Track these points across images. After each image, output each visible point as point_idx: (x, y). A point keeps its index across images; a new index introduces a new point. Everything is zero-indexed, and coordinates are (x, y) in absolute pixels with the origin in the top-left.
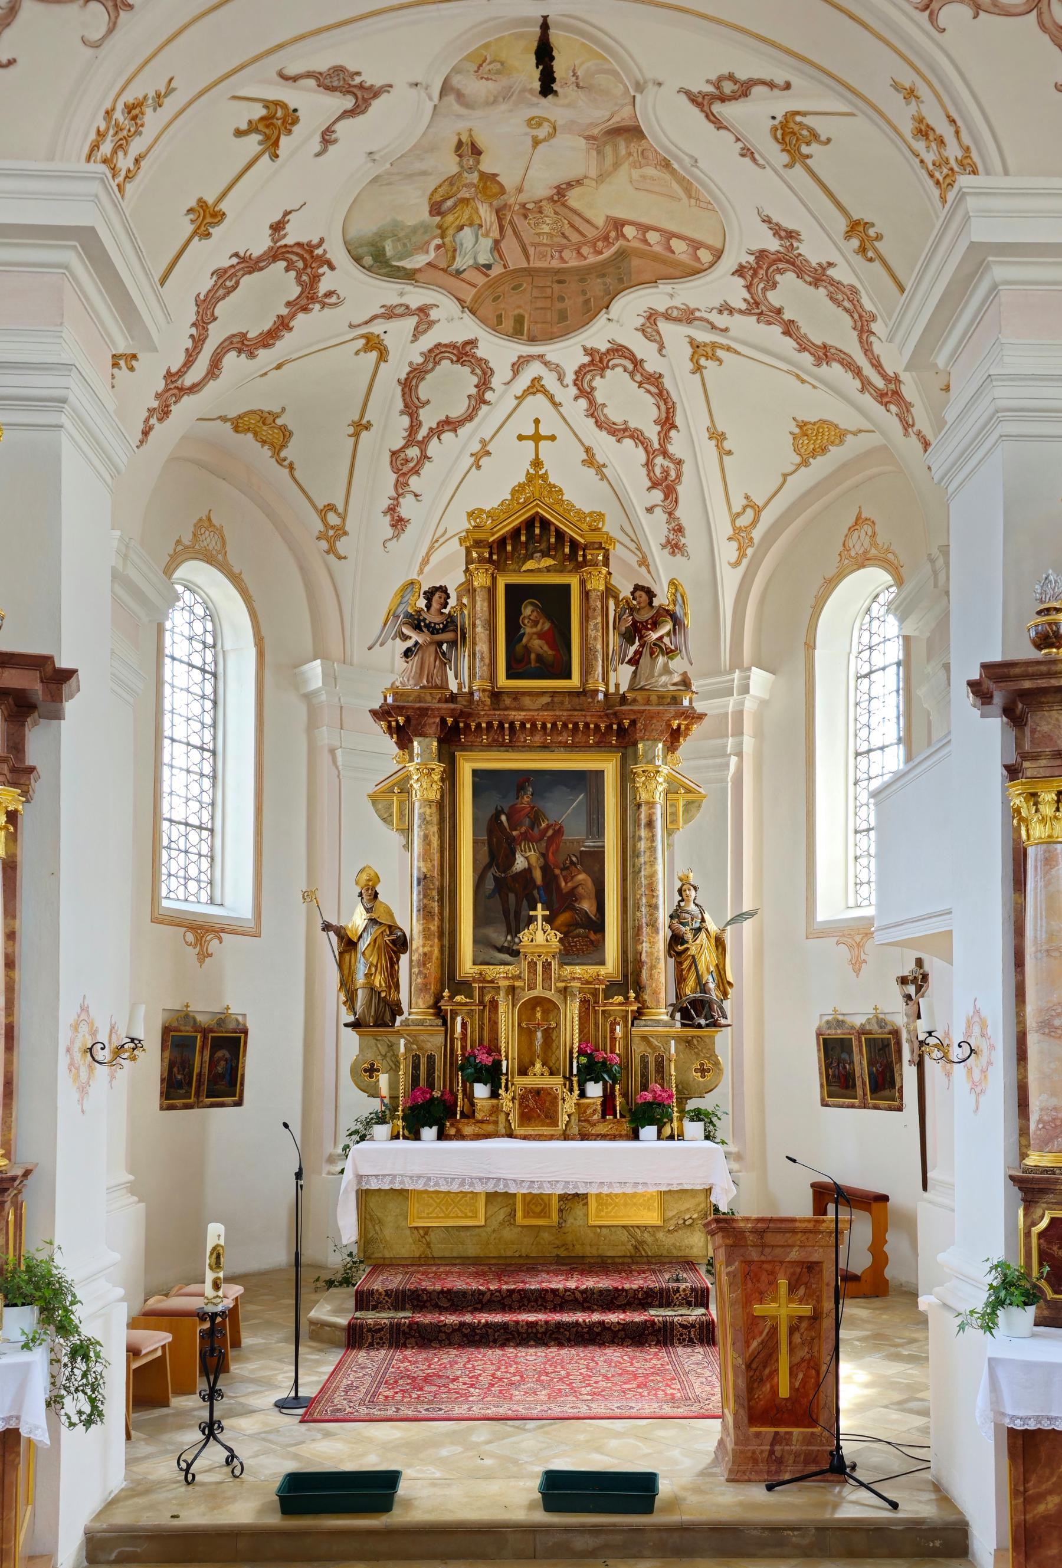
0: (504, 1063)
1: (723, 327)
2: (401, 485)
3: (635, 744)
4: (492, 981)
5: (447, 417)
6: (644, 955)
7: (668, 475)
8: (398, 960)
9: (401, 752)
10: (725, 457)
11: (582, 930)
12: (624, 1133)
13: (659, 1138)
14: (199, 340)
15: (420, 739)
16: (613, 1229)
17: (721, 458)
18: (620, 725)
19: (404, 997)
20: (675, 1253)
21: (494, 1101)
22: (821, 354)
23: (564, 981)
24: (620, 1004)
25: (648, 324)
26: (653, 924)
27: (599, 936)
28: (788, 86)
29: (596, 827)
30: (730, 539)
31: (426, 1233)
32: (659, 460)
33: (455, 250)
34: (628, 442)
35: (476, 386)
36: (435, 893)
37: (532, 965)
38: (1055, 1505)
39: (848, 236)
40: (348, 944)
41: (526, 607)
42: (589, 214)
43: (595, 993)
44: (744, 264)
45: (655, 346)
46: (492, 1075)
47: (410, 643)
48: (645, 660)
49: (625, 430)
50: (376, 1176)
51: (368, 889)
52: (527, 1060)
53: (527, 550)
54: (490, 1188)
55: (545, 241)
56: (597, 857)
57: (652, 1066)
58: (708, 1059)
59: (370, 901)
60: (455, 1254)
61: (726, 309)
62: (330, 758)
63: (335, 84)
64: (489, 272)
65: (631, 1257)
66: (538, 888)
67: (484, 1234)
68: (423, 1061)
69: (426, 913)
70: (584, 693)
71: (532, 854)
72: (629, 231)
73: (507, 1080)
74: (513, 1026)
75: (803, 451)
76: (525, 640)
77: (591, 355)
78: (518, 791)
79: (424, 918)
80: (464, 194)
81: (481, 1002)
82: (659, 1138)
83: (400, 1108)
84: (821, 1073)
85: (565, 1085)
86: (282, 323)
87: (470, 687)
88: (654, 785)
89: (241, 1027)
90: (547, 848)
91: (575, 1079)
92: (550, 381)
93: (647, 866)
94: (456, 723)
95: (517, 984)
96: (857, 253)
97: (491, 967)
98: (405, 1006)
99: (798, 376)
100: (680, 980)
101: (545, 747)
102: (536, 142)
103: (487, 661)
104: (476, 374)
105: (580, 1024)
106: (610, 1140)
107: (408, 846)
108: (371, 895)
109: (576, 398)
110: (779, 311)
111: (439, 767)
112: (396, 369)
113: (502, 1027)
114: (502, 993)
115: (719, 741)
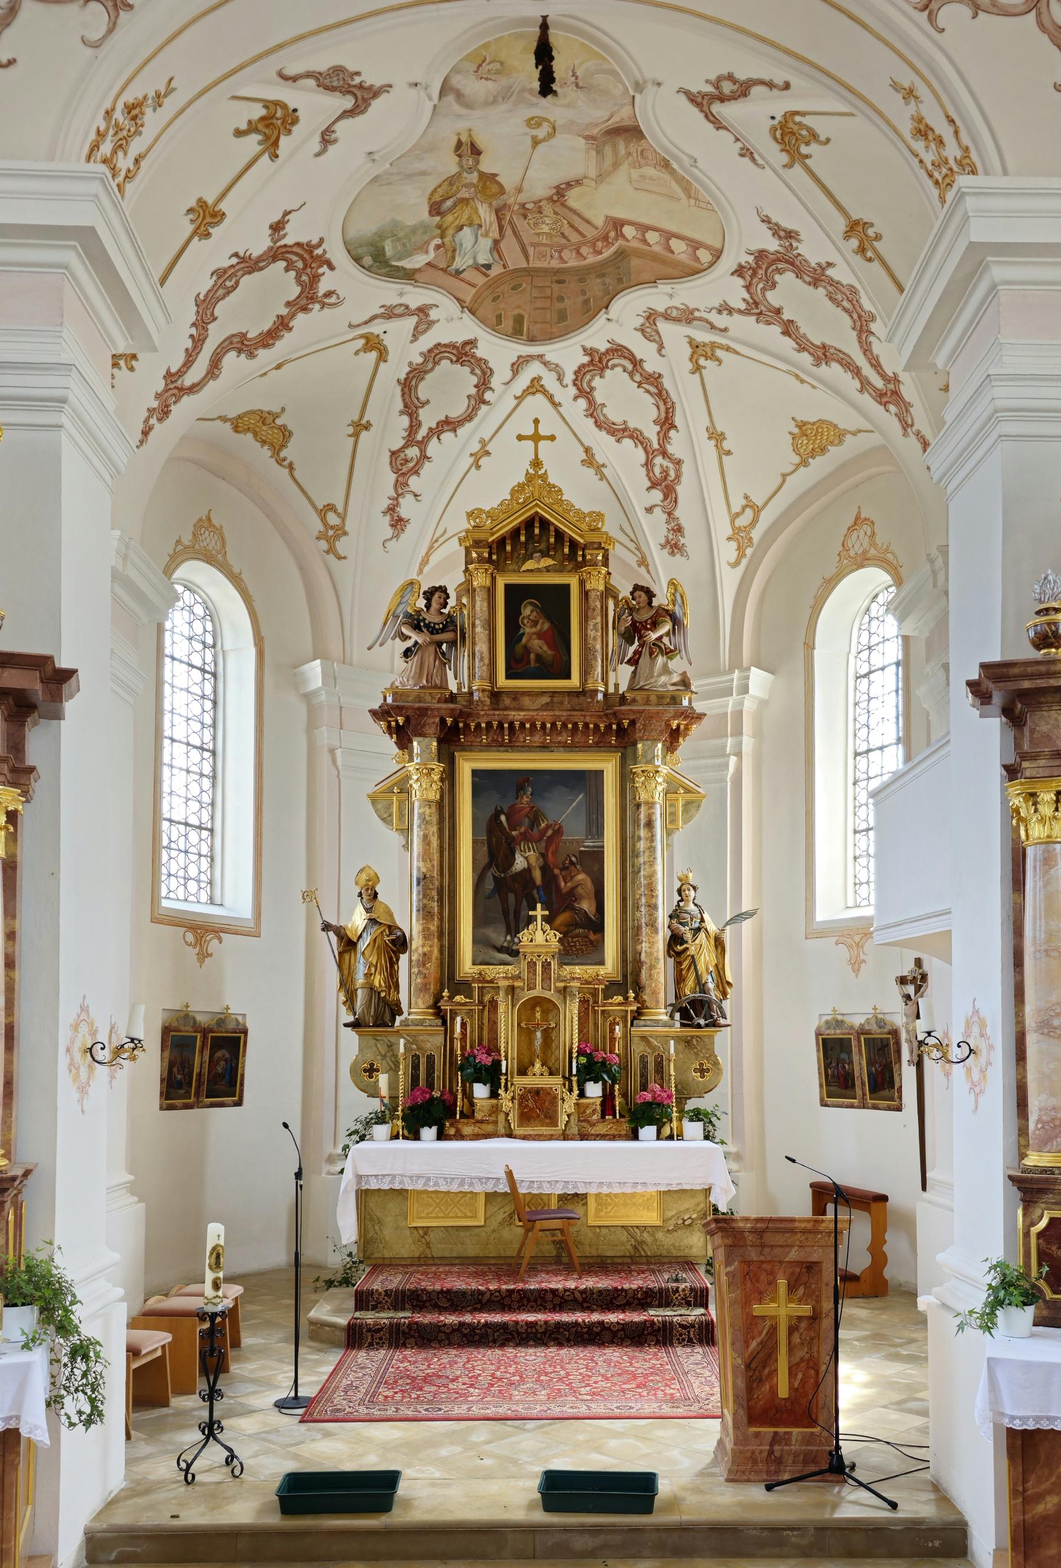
0: (504, 1063)
1: (723, 327)
2: (401, 485)
3: (635, 744)
4: (492, 981)
5: (447, 417)
6: (643, 955)
7: (668, 475)
8: (398, 960)
10: (724, 457)
11: (581, 930)
12: (623, 1133)
13: (658, 1138)
14: (199, 340)
15: (420, 739)
16: (612, 1229)
17: (720, 458)
18: (619, 725)
19: (403, 997)
20: (675, 1253)
21: (494, 1101)
22: (820, 354)
23: (563, 981)
24: (619, 1004)
25: (648, 324)
26: (652, 924)
27: (598, 936)
28: (787, 86)
29: (596, 827)
30: (729, 539)
31: (426, 1233)
32: (659, 460)
33: (454, 250)
34: (628, 443)
35: (476, 386)
36: (434, 893)
37: (532, 965)
38: (1054, 1505)
39: (847, 236)
40: (348, 944)
41: (525, 607)
42: (588, 214)
43: (594, 993)
44: (743, 264)
45: (654, 346)
46: (491, 1075)
47: (409, 643)
48: (644, 660)
49: (624, 430)
50: (376, 1176)
51: (367, 889)
53: (526, 550)
54: (490, 1188)
55: (544, 241)
56: (596, 857)
57: (651, 1066)
58: (707, 1059)
59: (369, 901)
60: (454, 1255)
61: (725, 309)
63: (335, 84)
64: (488, 272)
65: (630, 1257)
66: (538, 888)
68: (423, 1061)
69: (426, 913)
70: (584, 693)
71: (532, 854)
72: (629, 231)
73: (506, 1080)
74: (512, 1026)
75: (802, 451)
76: (524, 640)
77: (590, 355)
78: (518, 791)
79: (424, 918)
80: (464, 194)
82: (658, 1138)
83: (400, 1109)
84: (820, 1073)
85: (564, 1085)
86: (282, 323)
87: (470, 687)
88: (653, 785)
89: (240, 1027)
90: (547, 848)
91: (574, 1079)
92: (549, 381)
93: (647, 866)
94: (456, 722)
95: (516, 984)
96: (857, 253)
97: (491, 967)
98: (404, 1006)
99: (797, 376)
100: (680, 980)
101: (544, 747)
102: (536, 142)
103: (487, 661)
104: (475, 374)
105: (580, 1024)
106: (610, 1140)
107: (407, 846)
108: (370, 895)
109: (576, 398)
110: (778, 311)
111: (438, 767)
112: (395, 369)
114: (501, 993)
115: (718, 741)
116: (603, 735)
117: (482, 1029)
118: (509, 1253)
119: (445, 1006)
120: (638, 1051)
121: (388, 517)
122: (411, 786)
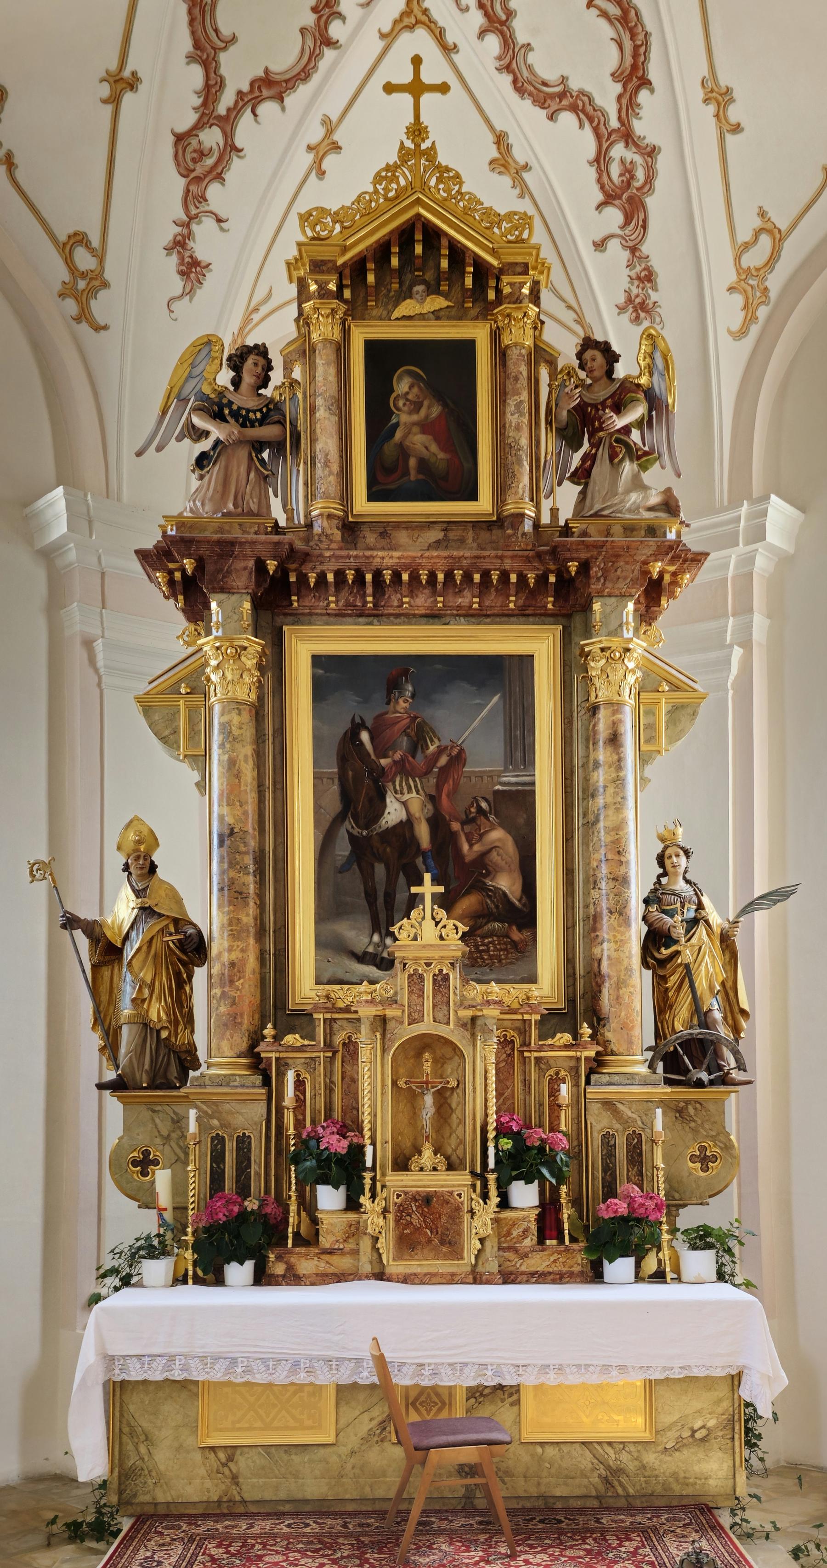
0: (369, 1150)
2: (194, 199)
3: (587, 608)
4: (347, 1010)
5: (267, 71)
6: (605, 964)
7: (632, 177)
8: (190, 977)
9: (192, 627)
10: (729, 137)
11: (497, 925)
12: (577, 1269)
13: (639, 1278)
15: (222, 596)
16: (565, 1449)
17: (722, 140)
19: (200, 1038)
20: (677, 1489)
21: (352, 1216)
24: (567, 1047)
26: (620, 911)
27: (526, 934)
29: (520, 749)
30: (731, 289)
31: (230, 1459)
32: (618, 151)
34: (567, 118)
36: (249, 860)
37: (416, 980)
40: (108, 952)
41: (400, 379)
43: (523, 1029)
46: (348, 1171)
47: (205, 445)
49: (562, 95)
50: (140, 1357)
51: (137, 858)
52: (409, 1144)
53: (401, 283)
54: (345, 1376)
56: (517, 806)
57: (621, 1153)
58: (713, 1138)
59: (142, 877)
60: (282, 1495)
62: (85, 656)
65: (597, 1497)
66: (424, 854)
67: (334, 1459)
68: (230, 1147)
69: (233, 894)
70: (501, 523)
71: (416, 800)
73: (374, 1179)
74: (383, 1085)
76: (398, 435)
78: (389, 692)
79: (230, 903)
81: (329, 1045)
82: (639, 1278)
83: (189, 1230)
85: (474, 1186)
87: (307, 514)
88: (621, 673)
90: (439, 787)
91: (492, 1177)
94: (283, 570)
95: (390, 1013)
97: (346, 987)
98: (202, 1054)
100: (663, 1006)
101: (433, 617)
103: (335, 467)
105: (498, 1081)
106: (554, 1282)
107: (203, 786)
108: (143, 868)
109: (482, 34)
111: (254, 645)
113: (365, 1087)
114: (365, 1029)
115: (713, 625)
116: (533, 593)
117: (331, 1090)
118: (380, 1493)
119: (268, 1052)
120: (597, 1127)
121: (174, 259)
122: (208, 679)
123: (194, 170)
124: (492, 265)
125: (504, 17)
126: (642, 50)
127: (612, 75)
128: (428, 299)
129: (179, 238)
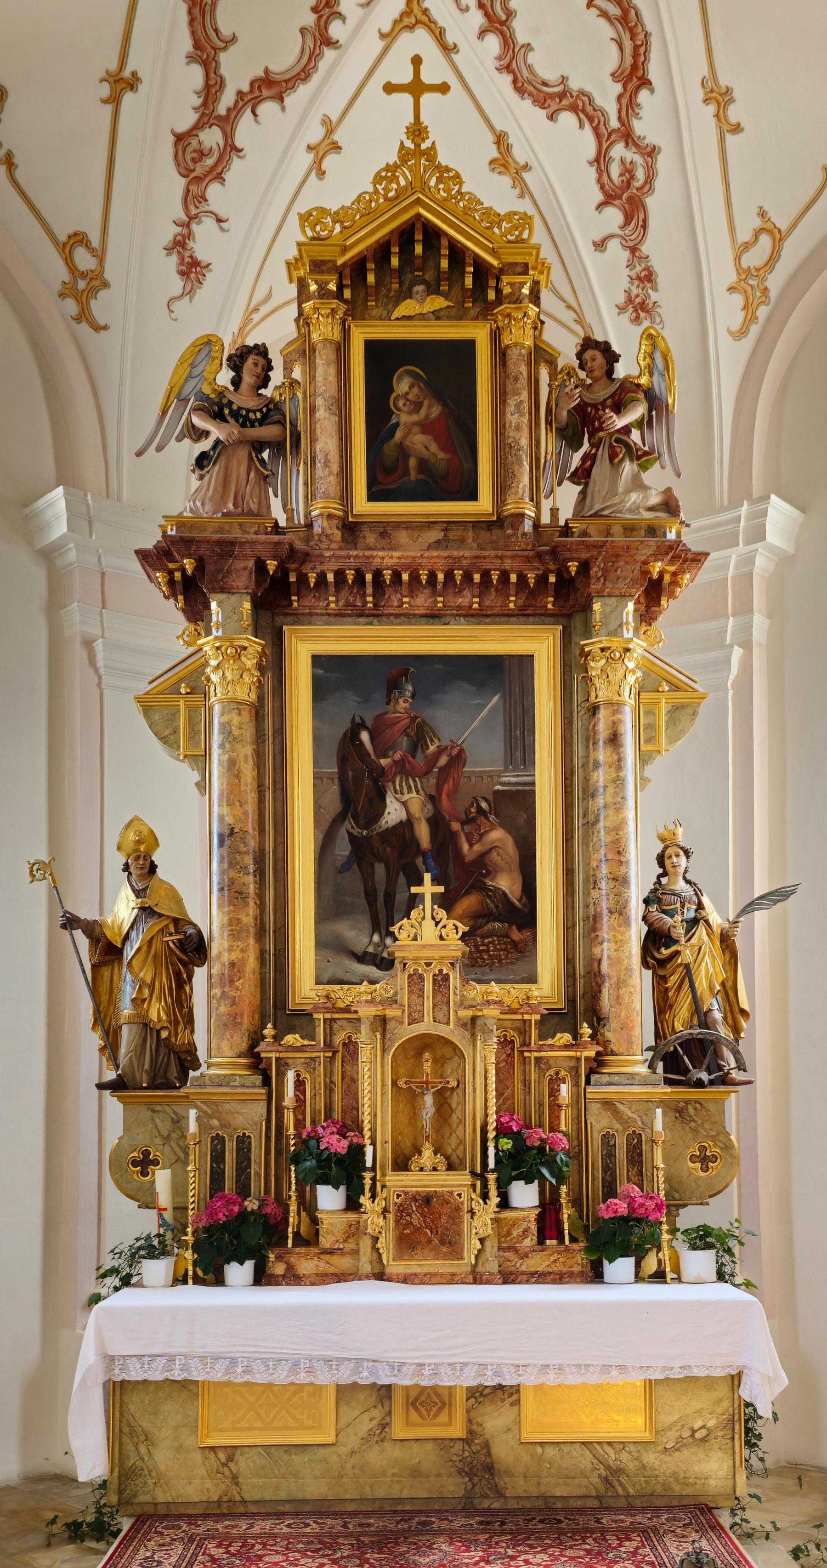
0: (369, 1150)
2: (194, 200)
3: (587, 608)
4: (347, 1010)
5: (267, 71)
6: (605, 964)
7: (632, 177)
8: (190, 977)
9: (192, 627)
10: (729, 137)
11: (497, 925)
12: (577, 1269)
13: (639, 1278)
15: (222, 596)
16: (565, 1448)
17: (722, 140)
18: (562, 573)
19: (200, 1038)
20: (677, 1489)
21: (352, 1216)
23: (471, 1007)
24: (567, 1047)
26: (620, 911)
27: (526, 934)
29: (520, 749)
30: (731, 289)
31: (230, 1459)
32: (618, 151)
34: (567, 118)
36: (249, 860)
37: (416, 980)
40: (108, 952)
41: (400, 378)
43: (523, 1029)
46: (348, 1171)
47: (205, 445)
49: (562, 95)
50: (140, 1357)
51: (137, 858)
53: (401, 283)
54: (345, 1376)
56: (517, 806)
57: (621, 1153)
58: (713, 1138)
59: (142, 877)
60: (282, 1496)
62: (85, 656)
65: (597, 1497)
66: (424, 854)
67: (334, 1459)
68: (230, 1147)
69: (233, 894)
70: (501, 523)
71: (416, 800)
73: (374, 1179)
74: (383, 1086)
76: (398, 435)
78: (389, 692)
79: (230, 903)
81: (329, 1045)
82: (639, 1278)
83: (189, 1230)
85: (474, 1186)
87: (307, 514)
88: (621, 673)
90: (439, 787)
91: (492, 1177)
93: (611, 812)
94: (283, 570)
95: (390, 1013)
97: (346, 987)
98: (202, 1054)
100: (663, 1006)
101: (433, 617)
103: (335, 467)
105: (498, 1081)
106: (554, 1282)
107: (203, 786)
108: (143, 868)
109: (482, 34)
111: (254, 645)
114: (365, 1029)
116: (533, 594)
117: (331, 1090)
119: (268, 1052)
121: (174, 259)
122: (208, 679)
123: (194, 170)
124: (491, 265)
125: (504, 17)
126: (642, 50)
127: (612, 75)
128: (428, 299)
129: (179, 238)
